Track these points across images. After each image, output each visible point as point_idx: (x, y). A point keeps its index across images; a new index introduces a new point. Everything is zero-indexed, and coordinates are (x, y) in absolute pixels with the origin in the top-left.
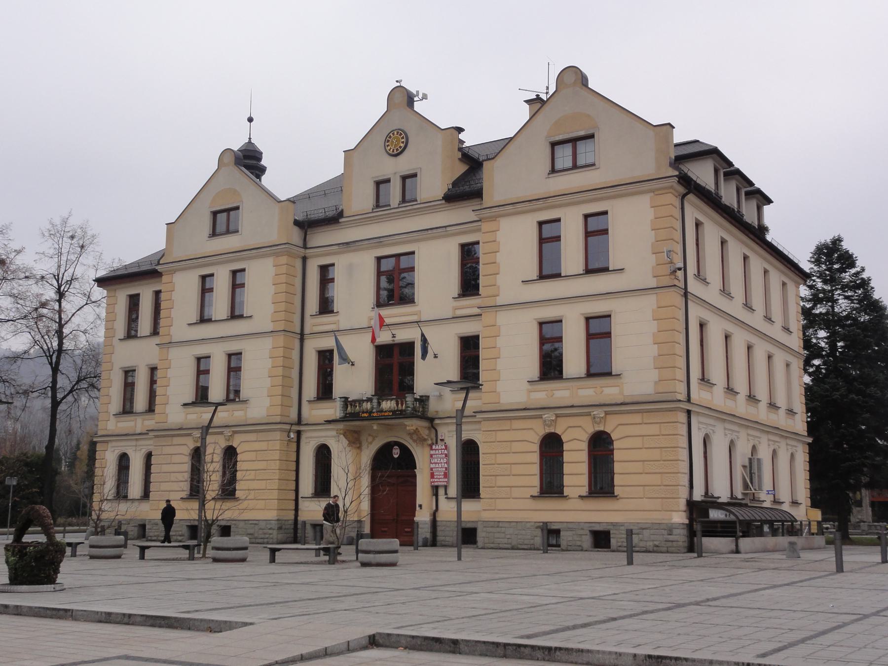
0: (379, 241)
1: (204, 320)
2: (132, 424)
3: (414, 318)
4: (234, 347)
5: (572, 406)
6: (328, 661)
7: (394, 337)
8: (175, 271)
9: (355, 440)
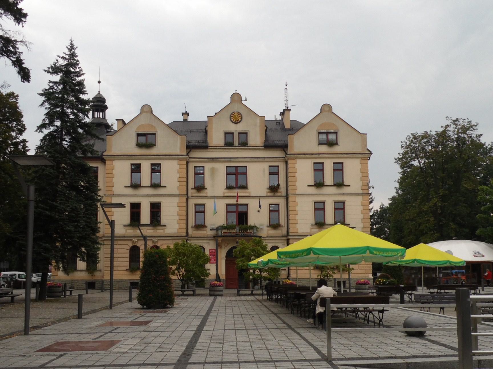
0: (230, 159)
2: (162, 231)
3: (247, 195)
6: (77, 368)
8: (114, 160)
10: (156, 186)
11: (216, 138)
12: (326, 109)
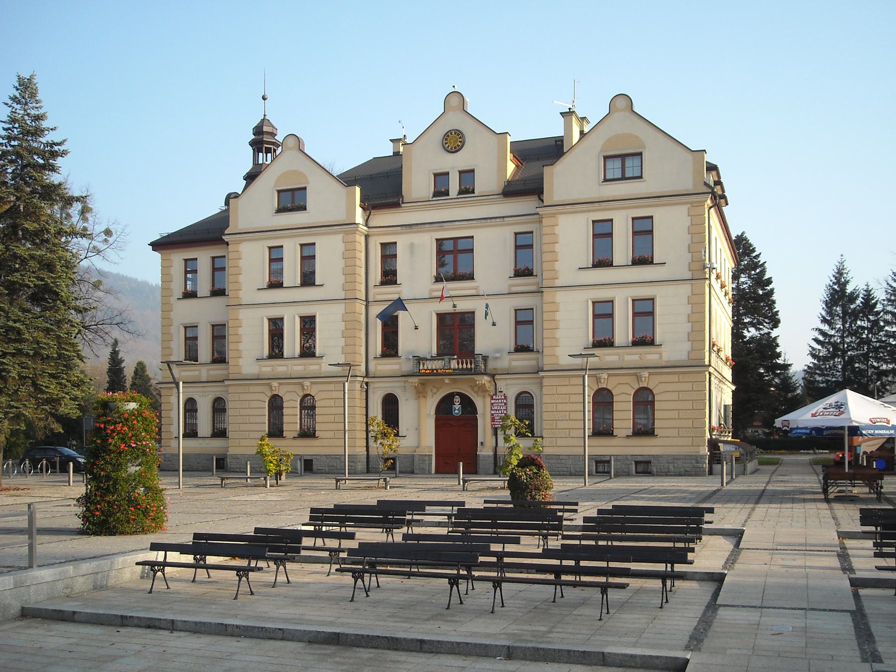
1: (275, 284)
2: (197, 373)
3: (473, 292)
4: (307, 311)
5: (622, 368)
7: (454, 306)
8: (242, 241)
9: (420, 393)
10: (219, 292)
11: (417, 183)
12: (622, 103)
